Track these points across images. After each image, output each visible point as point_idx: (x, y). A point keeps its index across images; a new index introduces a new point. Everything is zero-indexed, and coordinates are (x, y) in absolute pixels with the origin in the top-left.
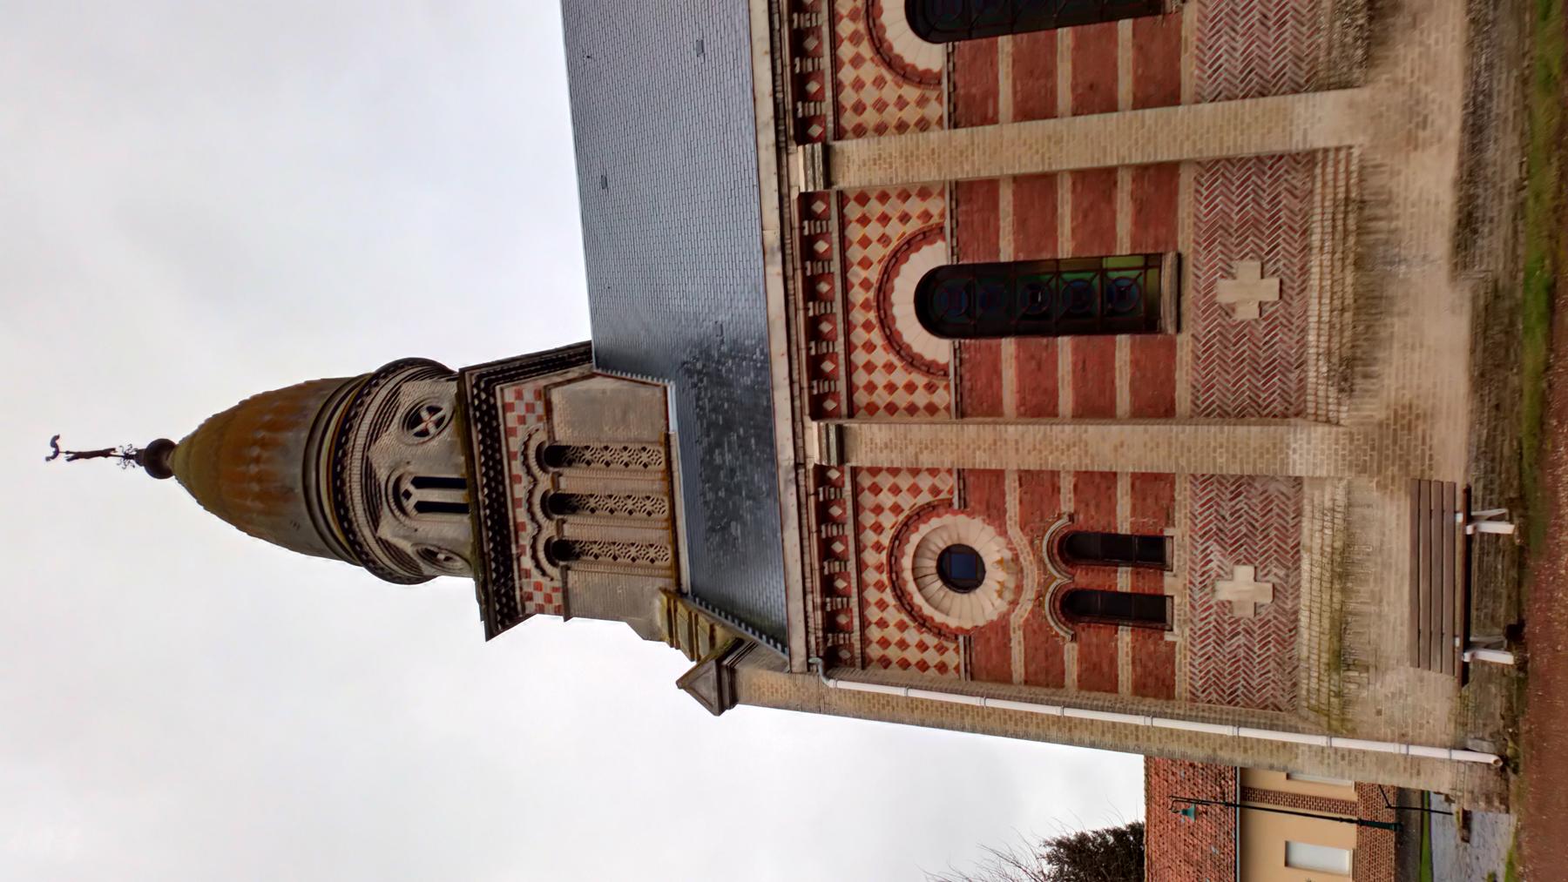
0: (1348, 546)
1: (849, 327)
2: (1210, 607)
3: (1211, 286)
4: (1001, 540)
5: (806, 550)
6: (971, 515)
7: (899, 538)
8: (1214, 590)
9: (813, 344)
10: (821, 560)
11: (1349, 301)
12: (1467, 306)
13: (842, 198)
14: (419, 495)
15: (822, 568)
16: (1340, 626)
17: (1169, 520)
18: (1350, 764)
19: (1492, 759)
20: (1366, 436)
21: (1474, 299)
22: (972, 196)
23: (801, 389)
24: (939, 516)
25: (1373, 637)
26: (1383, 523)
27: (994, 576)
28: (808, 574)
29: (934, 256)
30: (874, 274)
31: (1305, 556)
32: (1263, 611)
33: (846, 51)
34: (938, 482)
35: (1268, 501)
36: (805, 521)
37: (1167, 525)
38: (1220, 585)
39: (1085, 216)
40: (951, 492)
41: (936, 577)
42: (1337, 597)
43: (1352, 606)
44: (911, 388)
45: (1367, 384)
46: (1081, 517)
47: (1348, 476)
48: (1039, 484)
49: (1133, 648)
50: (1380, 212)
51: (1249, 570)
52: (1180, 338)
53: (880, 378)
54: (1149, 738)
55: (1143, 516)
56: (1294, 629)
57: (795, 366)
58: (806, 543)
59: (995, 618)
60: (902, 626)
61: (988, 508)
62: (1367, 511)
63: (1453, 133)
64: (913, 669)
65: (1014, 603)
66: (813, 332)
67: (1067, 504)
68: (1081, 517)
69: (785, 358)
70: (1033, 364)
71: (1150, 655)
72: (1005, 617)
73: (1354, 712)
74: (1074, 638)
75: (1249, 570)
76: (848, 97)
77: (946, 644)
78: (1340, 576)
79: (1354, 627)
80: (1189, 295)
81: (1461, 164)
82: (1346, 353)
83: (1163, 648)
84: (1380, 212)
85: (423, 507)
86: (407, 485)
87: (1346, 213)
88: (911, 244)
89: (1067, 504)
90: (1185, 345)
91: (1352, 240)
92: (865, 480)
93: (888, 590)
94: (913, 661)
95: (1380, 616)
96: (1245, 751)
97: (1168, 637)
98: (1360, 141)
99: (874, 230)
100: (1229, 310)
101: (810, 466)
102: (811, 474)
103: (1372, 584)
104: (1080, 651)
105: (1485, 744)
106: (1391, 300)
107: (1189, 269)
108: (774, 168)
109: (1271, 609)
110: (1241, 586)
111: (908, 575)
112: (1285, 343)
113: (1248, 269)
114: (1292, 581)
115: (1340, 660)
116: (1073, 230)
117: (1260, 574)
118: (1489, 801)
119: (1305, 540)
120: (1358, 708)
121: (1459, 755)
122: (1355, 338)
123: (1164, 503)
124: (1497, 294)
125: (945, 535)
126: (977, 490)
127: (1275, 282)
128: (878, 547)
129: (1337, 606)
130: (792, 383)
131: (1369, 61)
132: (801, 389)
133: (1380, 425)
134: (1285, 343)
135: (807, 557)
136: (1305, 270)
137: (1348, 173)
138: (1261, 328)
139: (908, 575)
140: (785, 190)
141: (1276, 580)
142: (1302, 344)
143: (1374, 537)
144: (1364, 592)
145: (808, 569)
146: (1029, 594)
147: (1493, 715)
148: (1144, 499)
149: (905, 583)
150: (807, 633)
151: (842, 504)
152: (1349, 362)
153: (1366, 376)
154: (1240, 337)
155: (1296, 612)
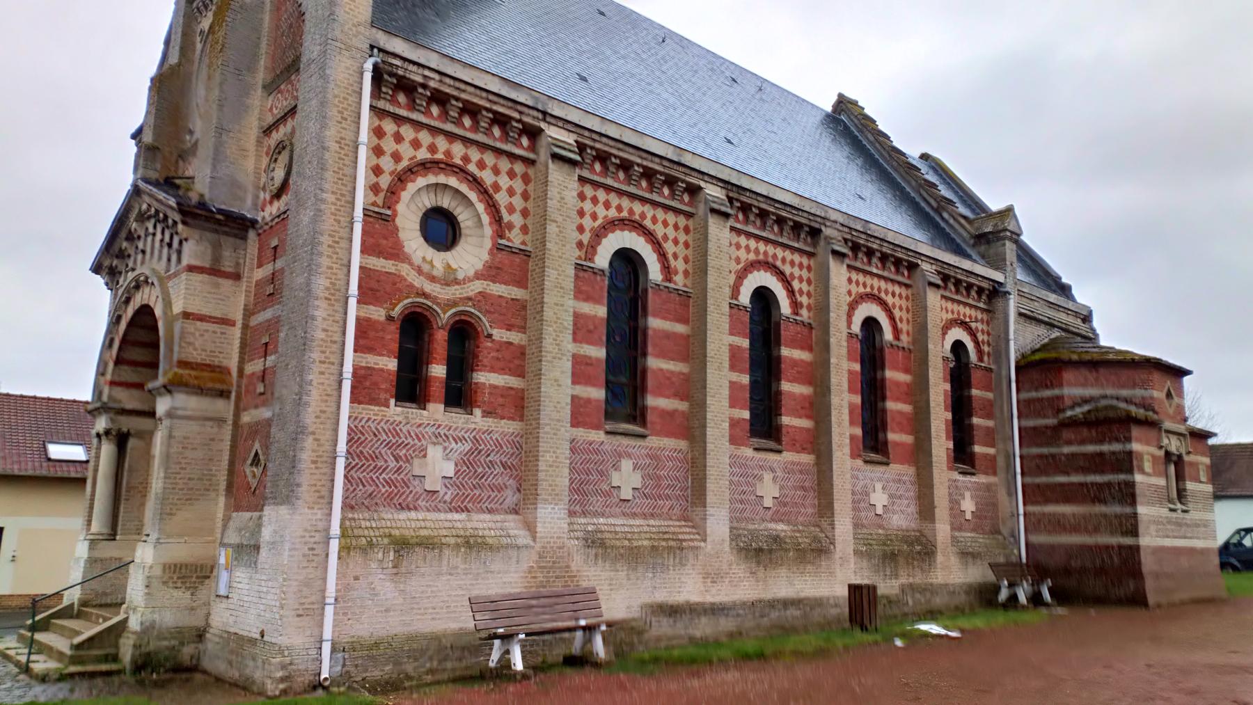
0: (491, 547)
2: (419, 440)
3: (629, 456)
4: (471, 273)
5: (478, 92)
6: (491, 252)
7: (476, 182)
8: (434, 444)
9: (618, 161)
10: (465, 102)
11: (635, 543)
12: (630, 616)
15: (457, 99)
16: (429, 544)
17: (487, 414)
18: (304, 556)
19: (325, 674)
20: (562, 557)
21: (634, 619)
24: (491, 224)
25: (422, 570)
26: (506, 572)
27: (440, 260)
28: (457, 84)
29: (655, 272)
31: (463, 516)
32: (416, 482)
33: (425, 137)
34: (516, 231)
35: (500, 489)
36: (502, 101)
37: (484, 412)
38: (439, 449)
39: (669, 379)
40: (509, 240)
41: (434, 204)
42: (452, 541)
43: (447, 552)
45: (592, 557)
46: (489, 344)
47: (538, 546)
48: (520, 315)
49: (382, 370)
50: (677, 560)
51: (451, 474)
52: (602, 433)
53: (504, 181)
54: (322, 373)
55: (490, 394)
56: (402, 508)
57: (611, 143)
58: (484, 94)
59: (406, 249)
61: (498, 268)
62: (514, 560)
63: (709, 599)
65: (419, 271)
66: (626, 166)
67: (499, 334)
68: (489, 344)
69: (617, 137)
70: (591, 327)
71: (376, 384)
72: (406, 259)
73: (357, 557)
74: (390, 318)
75: (451, 474)
77: (382, 195)
78: (467, 542)
79: (430, 555)
80: (625, 441)
81: (697, 604)
82: (608, 543)
83: (383, 396)
84: (677, 560)
87: (651, 539)
89: (499, 334)
90: (598, 436)
91: (626, 543)
93: (429, 156)
95: (439, 574)
96: (314, 462)
97: (392, 401)
98: (708, 547)
100: (616, 467)
101: (543, 125)
102: (536, 123)
103: (462, 566)
104: (377, 322)
105: (339, 668)
106: (635, 569)
107: (639, 442)
108: (719, 176)
109: (418, 489)
110: (438, 466)
111: (442, 179)
112: (597, 503)
113: (636, 480)
114: (440, 506)
115: (402, 545)
116: (661, 370)
117: (446, 481)
118: (282, 680)
119: (475, 516)
120: (360, 559)
121: (327, 648)
122: (617, 548)
123: (499, 411)
124: (640, 633)
125: (469, 223)
126: (517, 263)
127: (630, 497)
128: (466, 159)
129: (444, 540)
130: (601, 135)
131: (740, 550)
132: (594, 140)
133: (568, 567)
134: (597, 503)
135: (471, 89)
136: (634, 515)
137: (691, 540)
138: (605, 487)
139: (442, 179)
140: (706, 178)
141: (442, 493)
142: (596, 514)
143: (496, 566)
144: (458, 561)
145: (463, 86)
146: (428, 287)
147: (366, 671)
148: (502, 396)
149: (436, 174)
150: (404, 59)
152: (603, 544)
153: (596, 555)
154: (601, 473)
155: (416, 509)
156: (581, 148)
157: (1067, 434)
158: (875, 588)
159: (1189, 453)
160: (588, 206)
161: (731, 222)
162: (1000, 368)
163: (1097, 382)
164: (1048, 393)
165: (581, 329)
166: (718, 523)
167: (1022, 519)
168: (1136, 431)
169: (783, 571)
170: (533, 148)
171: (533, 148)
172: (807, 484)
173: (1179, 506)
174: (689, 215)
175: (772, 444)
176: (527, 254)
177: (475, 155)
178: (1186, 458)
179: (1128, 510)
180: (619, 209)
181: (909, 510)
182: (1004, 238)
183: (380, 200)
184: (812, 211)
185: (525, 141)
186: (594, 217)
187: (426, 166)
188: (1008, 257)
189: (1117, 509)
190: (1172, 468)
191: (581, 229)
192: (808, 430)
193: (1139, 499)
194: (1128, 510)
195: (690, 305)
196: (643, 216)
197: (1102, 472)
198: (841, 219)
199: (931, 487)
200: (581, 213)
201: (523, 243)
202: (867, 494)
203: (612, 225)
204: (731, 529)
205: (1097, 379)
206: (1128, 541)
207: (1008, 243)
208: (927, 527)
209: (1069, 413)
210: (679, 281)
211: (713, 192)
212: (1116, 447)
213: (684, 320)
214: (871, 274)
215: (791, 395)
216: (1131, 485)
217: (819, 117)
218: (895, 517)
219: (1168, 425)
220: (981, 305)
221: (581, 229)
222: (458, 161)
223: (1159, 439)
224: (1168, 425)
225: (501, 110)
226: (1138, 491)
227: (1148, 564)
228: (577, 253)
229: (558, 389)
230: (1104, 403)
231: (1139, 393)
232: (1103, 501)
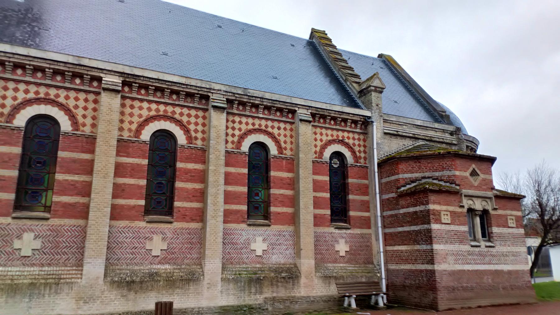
10: (277, 107)
13: (98, 94)
23: (10, 57)
29: (273, 150)
33: (154, 106)
39: (72, 185)
76: (137, 104)
92: (91, 97)
99: (81, 103)
108: (114, 70)
128: (266, 126)
131: (113, 282)
132: (10, 57)
156: (313, 115)
157: (402, 202)
159: (495, 209)
160: (230, 125)
161: (312, 123)
162: (371, 166)
163: (420, 170)
164: (393, 178)
165: (317, 186)
167: (382, 254)
168: (432, 197)
170: (293, 118)
171: (293, 118)
172: (194, 240)
173: (483, 244)
174: (292, 123)
175: (168, 218)
176: (367, 167)
177: (270, 123)
178: (492, 212)
179: (429, 247)
180: (332, 136)
181: (288, 252)
182: (371, 91)
183: (132, 134)
184: (198, 85)
185: (290, 116)
186: (321, 140)
187: (330, 143)
188: (373, 101)
189: (424, 247)
190: (478, 220)
191: (316, 146)
192: (289, 214)
193: (435, 240)
194: (429, 247)
195: (292, 164)
196: (174, 112)
197: (416, 224)
198: (223, 88)
199: (300, 238)
200: (316, 140)
201: (203, 145)
202: (249, 244)
203: (330, 143)
205: (420, 168)
206: (429, 267)
207: (373, 94)
208: (297, 261)
209: (403, 189)
210: (288, 153)
211: (108, 79)
212: (422, 208)
213: (289, 171)
214: (259, 118)
215: (354, 200)
216: (429, 231)
217: (305, 42)
218: (274, 257)
219: (465, 191)
220: (358, 130)
221: (316, 146)
222: (263, 128)
223: (461, 201)
224: (465, 191)
225: (279, 106)
226: (434, 235)
227: (442, 282)
228: (315, 156)
229: (216, 205)
230: (423, 181)
231: (446, 173)
232: (417, 242)
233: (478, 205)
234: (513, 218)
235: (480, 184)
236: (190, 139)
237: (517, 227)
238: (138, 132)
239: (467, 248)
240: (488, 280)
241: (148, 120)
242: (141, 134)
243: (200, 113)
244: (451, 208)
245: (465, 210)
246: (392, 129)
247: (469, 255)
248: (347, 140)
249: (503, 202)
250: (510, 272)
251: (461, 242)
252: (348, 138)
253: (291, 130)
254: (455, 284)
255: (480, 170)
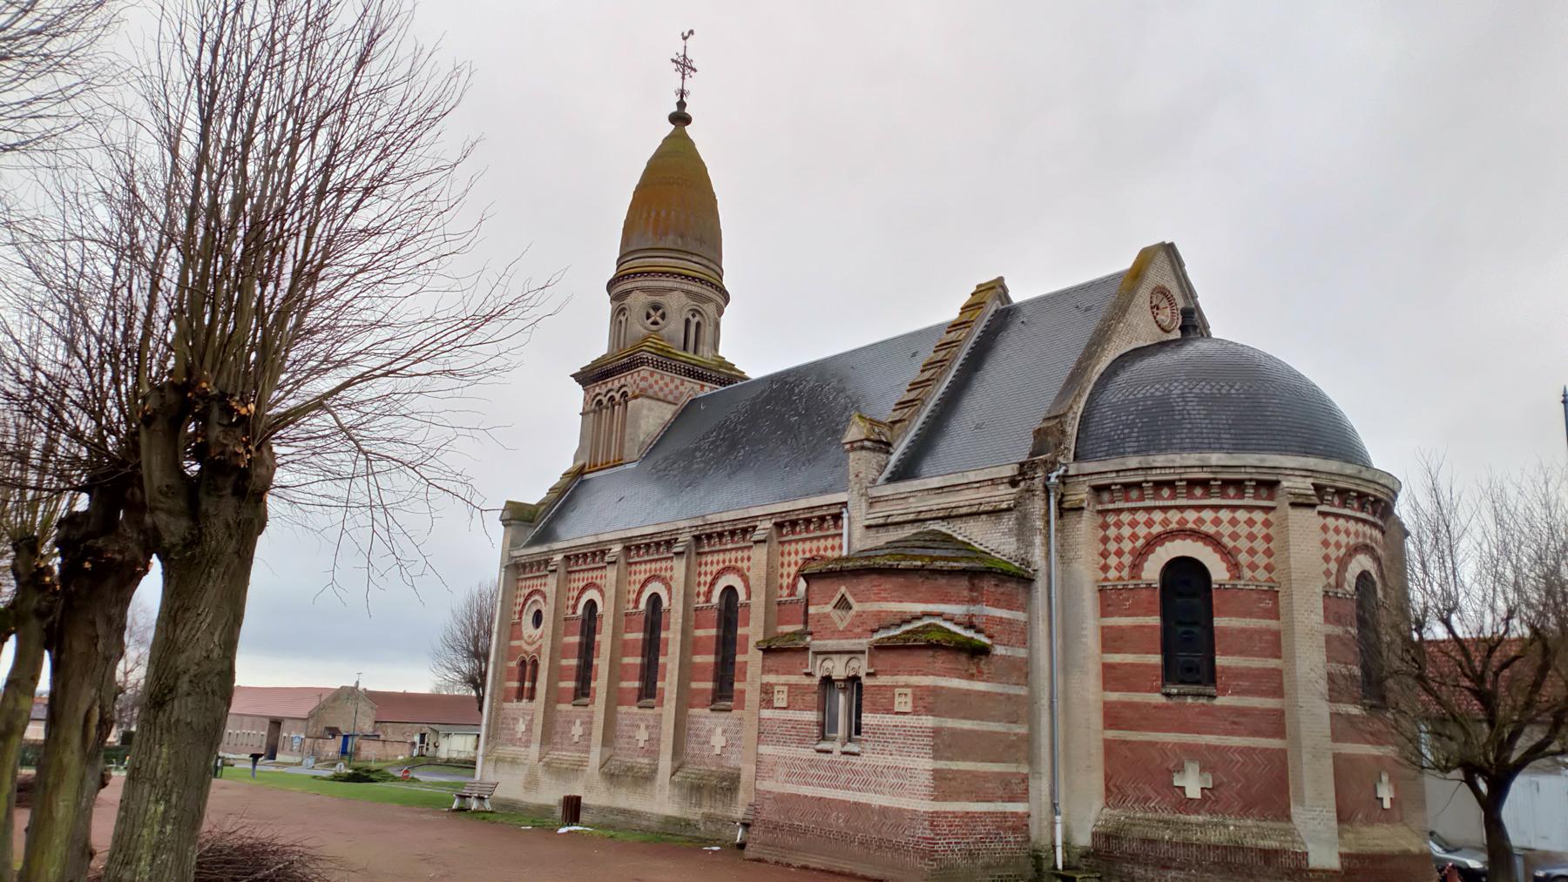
1: (1165, 509)
14: (694, 321)
22: (1271, 599)
30: (1209, 528)
33: (1158, 516)
44: (1119, 553)
53: (1126, 531)
60: (1235, 536)
64: (1101, 547)
76: (1126, 517)
85: (687, 322)
86: (697, 318)
88: (1228, 554)
94: (1123, 545)
99: (1243, 530)
131: (604, 773)
151: (1204, 496)
158: (579, 798)
166: (595, 757)
169: (624, 790)
178: (866, 681)
187: (720, 573)
200: (1326, 544)
204: (1289, 818)
222: (1190, 525)
233: (838, 669)
234: (908, 691)
235: (852, 624)
236: (1234, 567)
237: (915, 712)
238: (1136, 567)
239: (808, 753)
240: (837, 821)
241: (1153, 543)
242: (1142, 570)
243: (1259, 516)
244: (793, 679)
245: (816, 681)
246: (1293, 499)
247: (811, 766)
248: (1140, 543)
249: (892, 657)
250: (884, 811)
251: (801, 742)
252: (1217, 522)
253: (1267, 524)
254: (780, 819)
255: (854, 595)
